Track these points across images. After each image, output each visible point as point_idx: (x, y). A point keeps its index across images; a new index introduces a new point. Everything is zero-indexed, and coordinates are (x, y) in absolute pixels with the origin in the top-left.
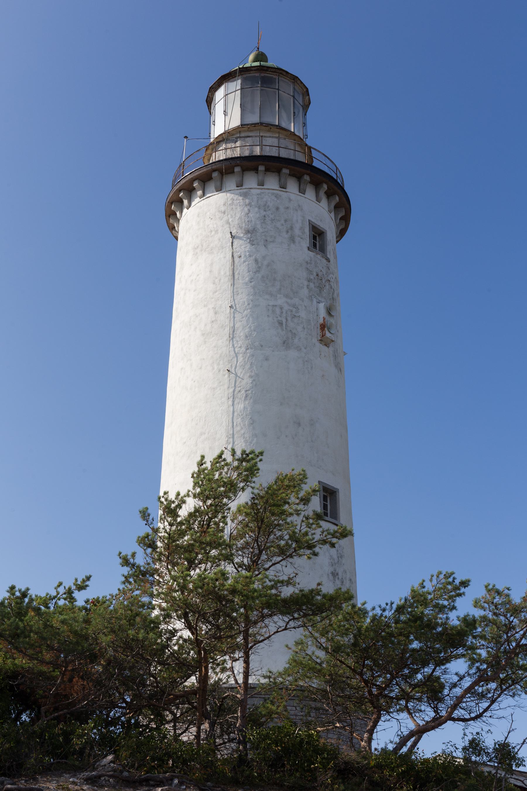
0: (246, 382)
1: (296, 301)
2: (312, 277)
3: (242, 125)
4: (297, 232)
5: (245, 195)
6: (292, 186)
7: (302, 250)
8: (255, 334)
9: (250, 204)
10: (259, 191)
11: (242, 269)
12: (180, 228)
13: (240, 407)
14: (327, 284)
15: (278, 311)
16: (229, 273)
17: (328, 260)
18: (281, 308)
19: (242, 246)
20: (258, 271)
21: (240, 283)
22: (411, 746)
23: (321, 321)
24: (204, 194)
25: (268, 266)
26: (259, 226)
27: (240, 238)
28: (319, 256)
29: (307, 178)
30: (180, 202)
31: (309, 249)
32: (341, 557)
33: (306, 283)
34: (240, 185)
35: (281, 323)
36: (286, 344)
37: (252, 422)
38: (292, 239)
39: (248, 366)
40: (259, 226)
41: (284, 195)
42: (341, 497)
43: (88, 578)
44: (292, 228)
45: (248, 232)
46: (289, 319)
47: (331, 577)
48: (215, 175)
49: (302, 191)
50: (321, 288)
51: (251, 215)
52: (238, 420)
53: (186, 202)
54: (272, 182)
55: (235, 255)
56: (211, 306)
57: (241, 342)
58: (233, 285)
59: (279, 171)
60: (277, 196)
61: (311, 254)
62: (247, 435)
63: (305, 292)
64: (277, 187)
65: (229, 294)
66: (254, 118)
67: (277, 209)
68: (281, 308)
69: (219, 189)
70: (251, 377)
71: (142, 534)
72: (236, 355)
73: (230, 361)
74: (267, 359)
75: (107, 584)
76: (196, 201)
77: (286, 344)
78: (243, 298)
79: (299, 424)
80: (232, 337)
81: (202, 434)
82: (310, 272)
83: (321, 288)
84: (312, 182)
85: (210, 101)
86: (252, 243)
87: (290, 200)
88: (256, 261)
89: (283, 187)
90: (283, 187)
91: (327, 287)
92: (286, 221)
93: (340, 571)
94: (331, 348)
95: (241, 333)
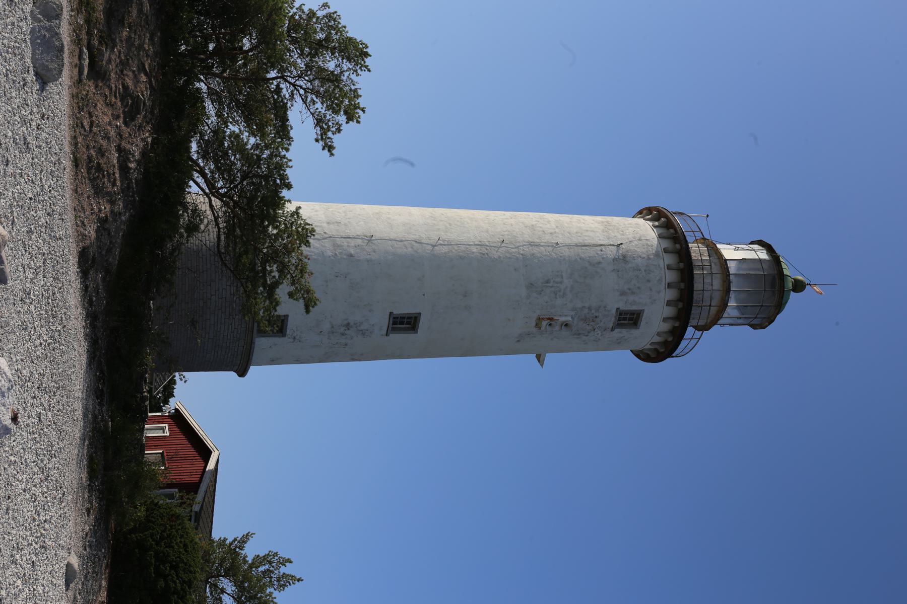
0: (495, 254)
2: (593, 311)
3: (726, 260)
4: (631, 298)
5: (657, 255)
6: (672, 294)
7: (616, 303)
8: (536, 261)
9: (649, 259)
10: (662, 266)
11: (591, 252)
12: (727, 328)
13: (474, 249)
14: (589, 328)
15: (558, 280)
16: (588, 241)
17: (612, 330)
18: (561, 282)
19: (611, 252)
20: (590, 263)
23: (555, 318)
24: (655, 227)
25: (596, 272)
26: (630, 265)
27: (618, 251)
28: (613, 319)
29: (680, 305)
30: (658, 220)
31: (618, 309)
32: (363, 334)
33: (587, 305)
34: (666, 251)
35: (548, 282)
36: (531, 286)
37: (461, 258)
38: (623, 294)
39: (508, 255)
40: (630, 265)
41: (663, 286)
44: (633, 293)
45: (624, 256)
46: (553, 289)
47: (346, 322)
48: (672, 231)
51: (640, 259)
52: (462, 248)
53: (657, 223)
54: (671, 276)
55: (602, 247)
56: (557, 230)
57: (527, 250)
58: (576, 245)
59: (682, 280)
60: (660, 281)
61: (614, 311)
62: (451, 254)
64: (668, 280)
65: (568, 242)
67: (649, 281)
68: (561, 282)
69: (660, 236)
70: (500, 257)
71: (364, 74)
72: (518, 247)
73: (511, 243)
74: (516, 270)
77: (531, 286)
78: (566, 252)
79: (465, 296)
80: (531, 244)
81: (450, 224)
82: (597, 310)
83: (585, 320)
84: (679, 310)
86: (615, 260)
87: (659, 292)
88: (600, 263)
89: (670, 286)
90: (670, 286)
91: (589, 328)
92: (639, 288)
93: (351, 332)
94: (535, 330)
95: (535, 250)
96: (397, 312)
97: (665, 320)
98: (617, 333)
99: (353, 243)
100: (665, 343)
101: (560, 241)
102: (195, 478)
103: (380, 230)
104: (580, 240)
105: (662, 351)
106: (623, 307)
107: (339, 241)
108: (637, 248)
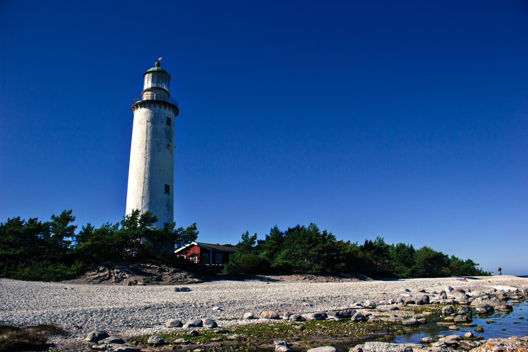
0: (148, 160)
1: (162, 139)
4: (163, 120)
5: (151, 109)
6: (163, 107)
11: (149, 130)
13: (147, 166)
19: (149, 124)
21: (148, 134)
22: (354, 346)
38: (162, 122)
42: (170, 187)
43: (195, 224)
49: (165, 109)
50: (168, 135)
57: (148, 150)
63: (164, 136)
65: (145, 137)
66: (155, 86)
69: (145, 108)
75: (416, 250)
76: (139, 109)
78: (149, 138)
85: (144, 76)
95: (148, 148)
96: (164, 191)
97: (169, 110)
98: (172, 125)
99: (144, 202)
100: (173, 109)
101: (145, 139)
102: (199, 248)
103: (140, 193)
104: (145, 135)
105: (175, 109)
106: (165, 123)
107: (143, 207)
108: (149, 115)
